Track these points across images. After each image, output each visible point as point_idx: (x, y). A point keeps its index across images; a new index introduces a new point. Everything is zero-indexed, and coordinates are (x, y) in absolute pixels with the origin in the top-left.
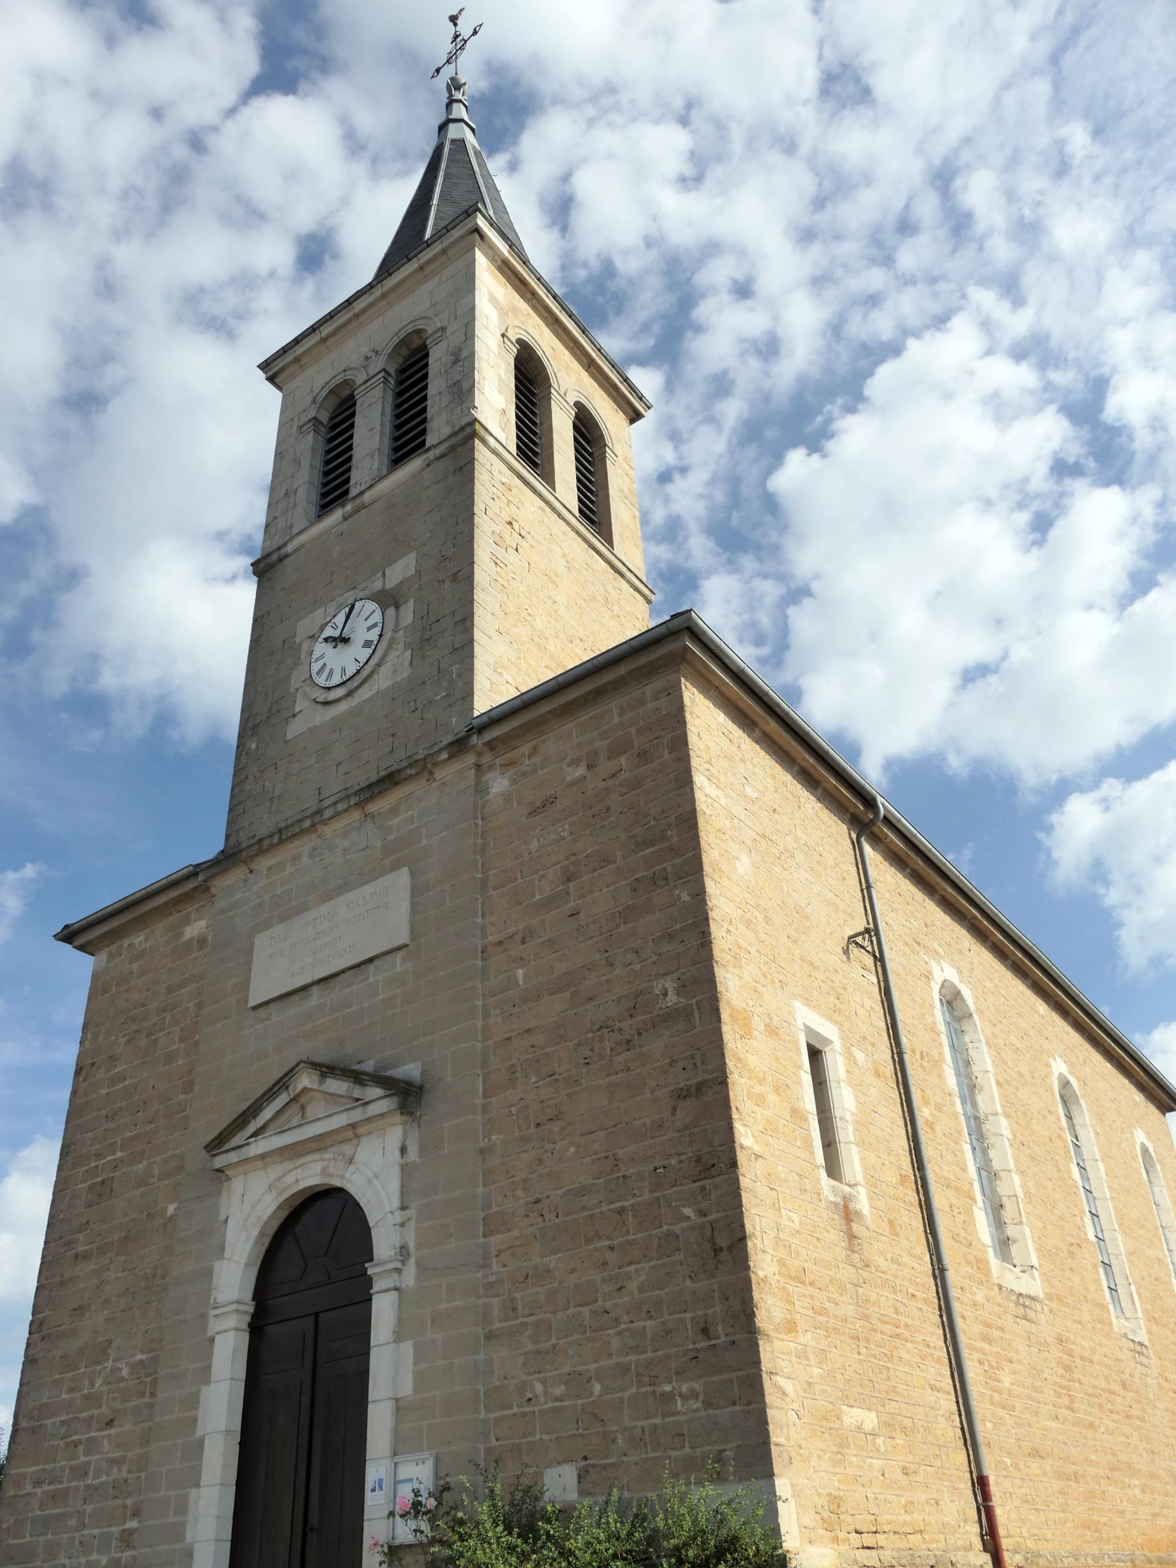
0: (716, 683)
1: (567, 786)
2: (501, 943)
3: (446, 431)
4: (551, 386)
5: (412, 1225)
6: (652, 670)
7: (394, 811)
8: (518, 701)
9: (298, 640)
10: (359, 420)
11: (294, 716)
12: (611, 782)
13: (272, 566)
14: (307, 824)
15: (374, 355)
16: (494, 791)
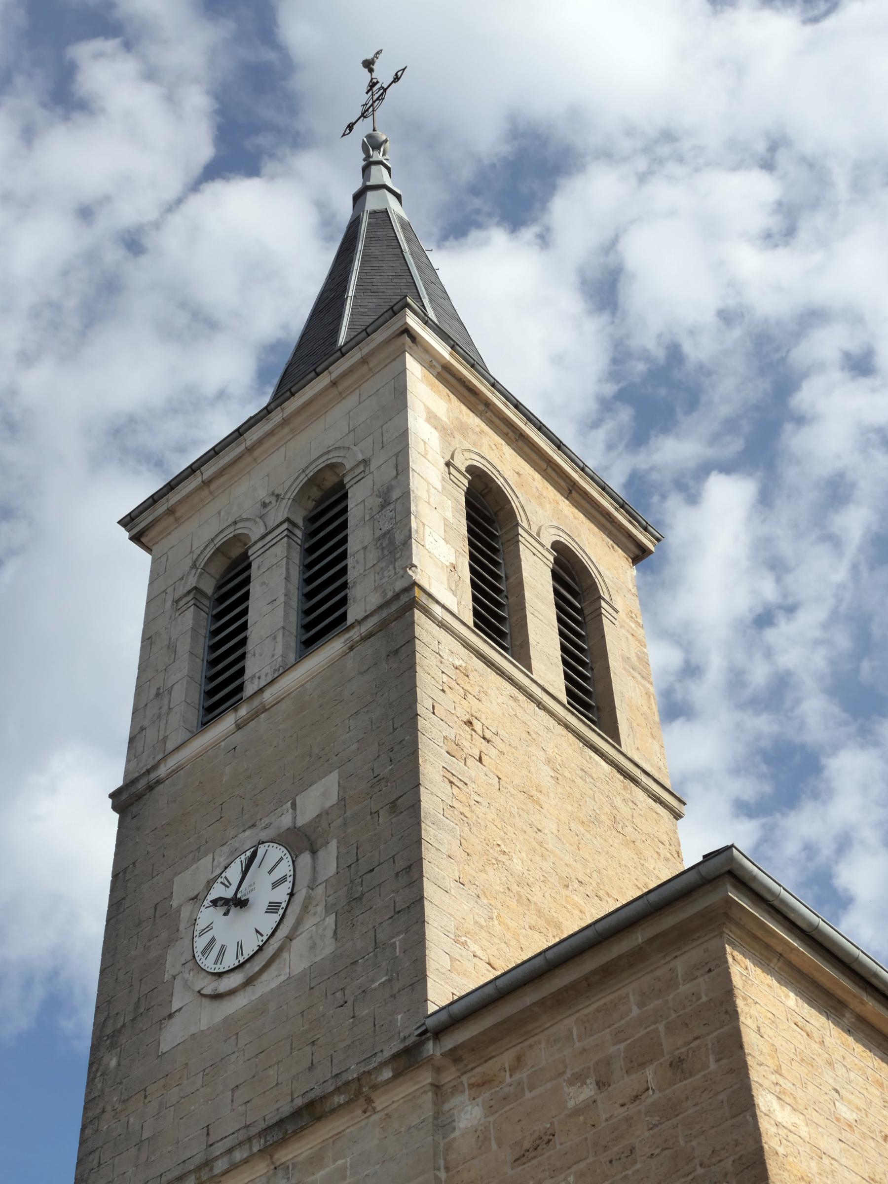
0: (779, 949)
1: (570, 1116)
3: (375, 600)
4: (517, 524)
6: (682, 936)
7: (316, 1160)
8: (490, 990)
9: (175, 903)
10: (255, 588)
11: (171, 1016)
12: (633, 1109)
13: (138, 797)
15: (273, 500)
16: (462, 1125)
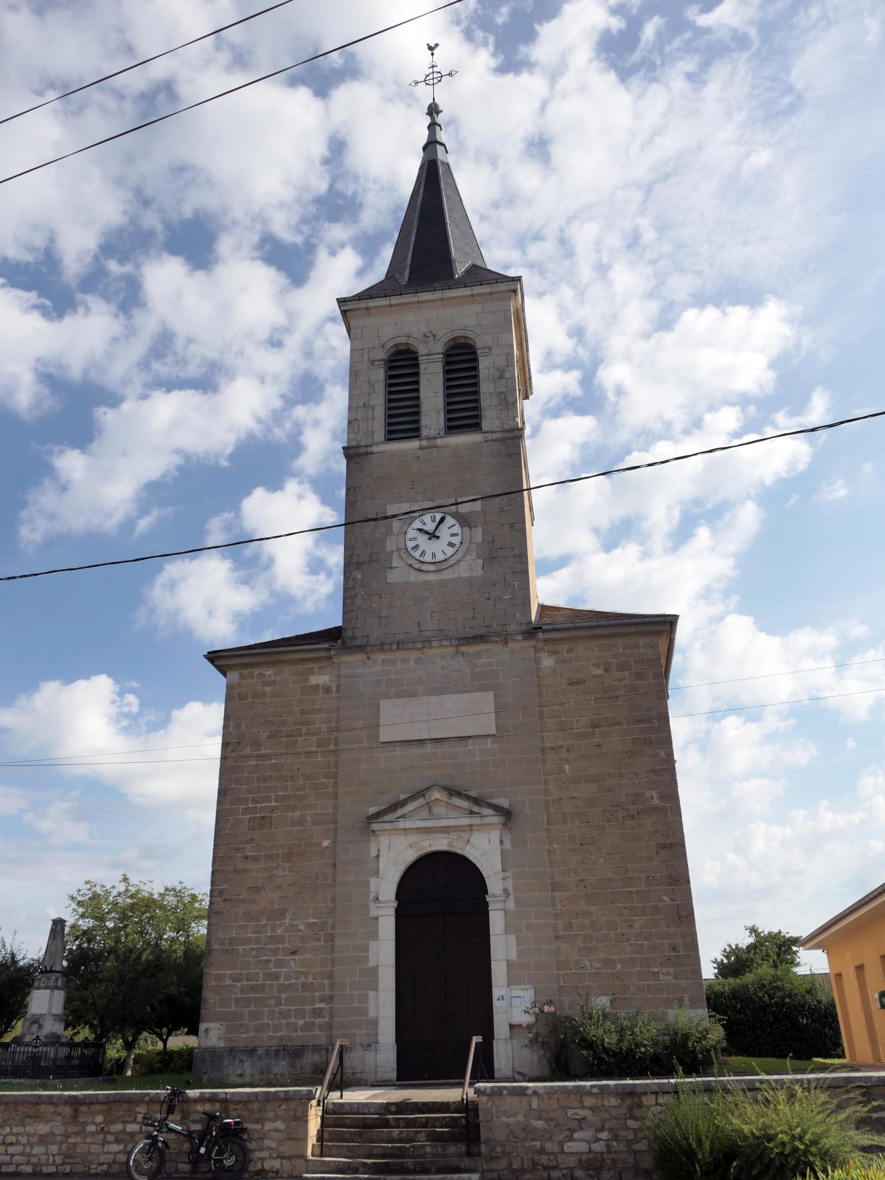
2: (553, 748)
5: (510, 880)
7: (478, 655)
11: (392, 568)
14: (419, 645)
